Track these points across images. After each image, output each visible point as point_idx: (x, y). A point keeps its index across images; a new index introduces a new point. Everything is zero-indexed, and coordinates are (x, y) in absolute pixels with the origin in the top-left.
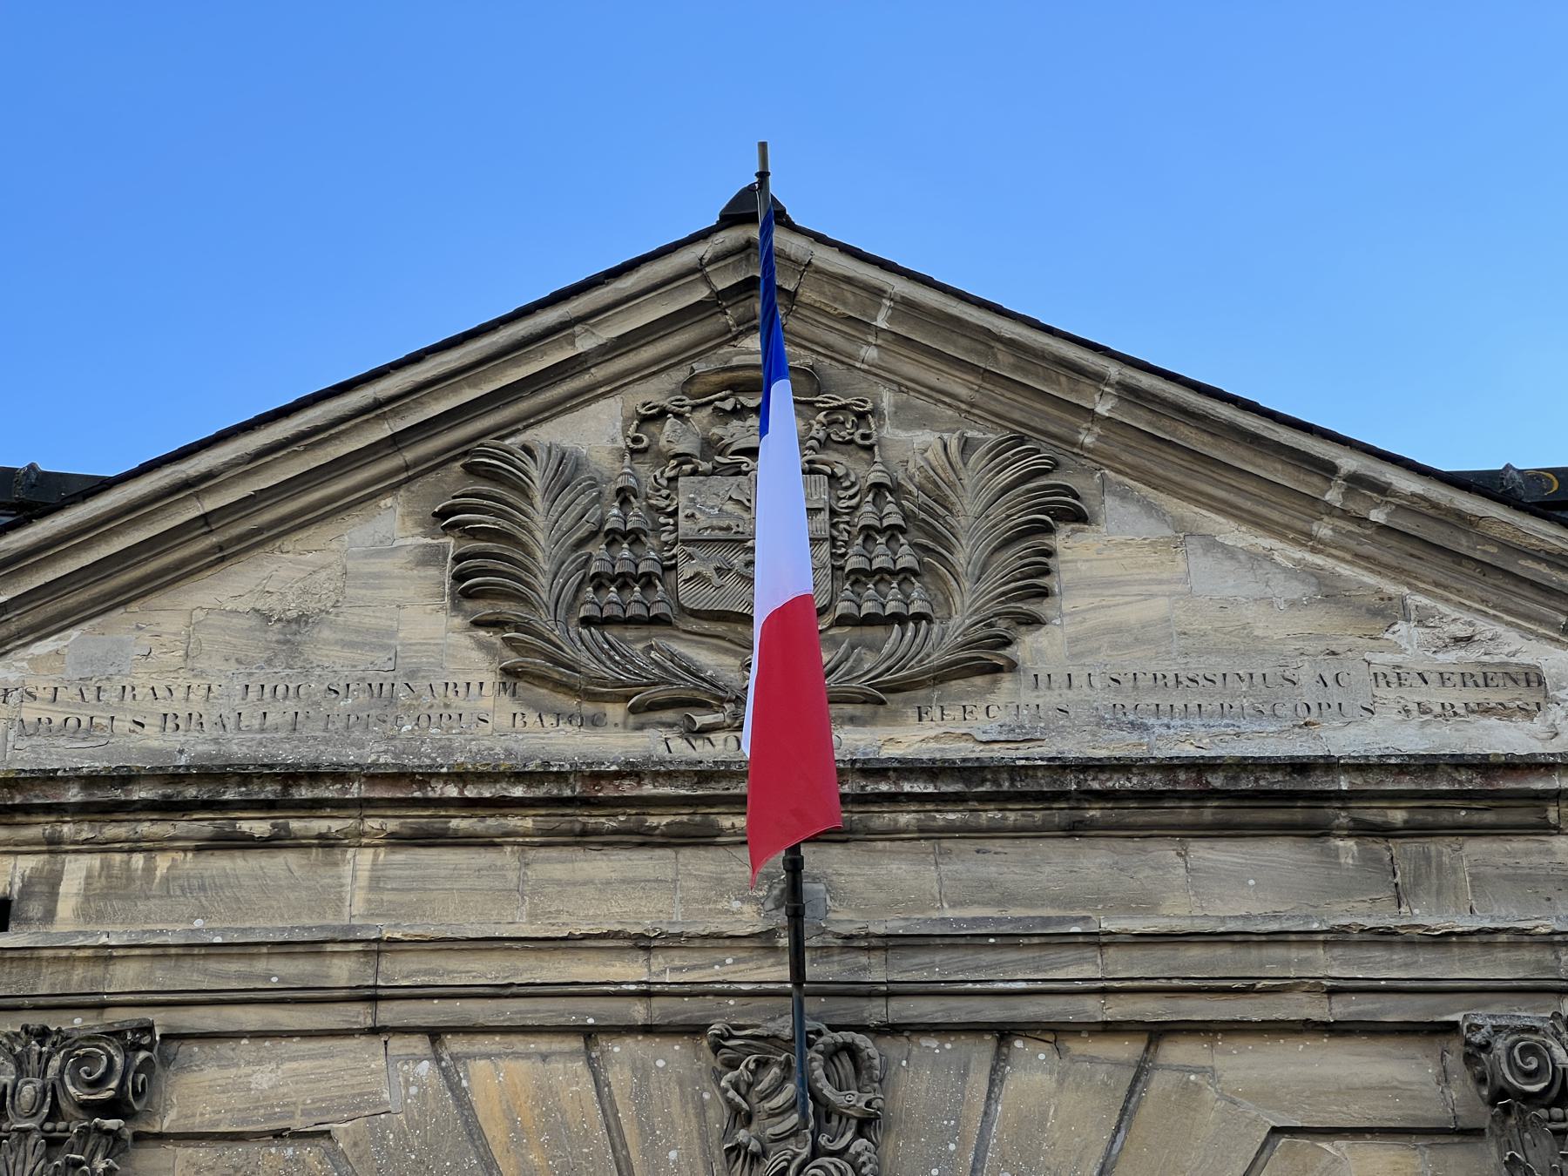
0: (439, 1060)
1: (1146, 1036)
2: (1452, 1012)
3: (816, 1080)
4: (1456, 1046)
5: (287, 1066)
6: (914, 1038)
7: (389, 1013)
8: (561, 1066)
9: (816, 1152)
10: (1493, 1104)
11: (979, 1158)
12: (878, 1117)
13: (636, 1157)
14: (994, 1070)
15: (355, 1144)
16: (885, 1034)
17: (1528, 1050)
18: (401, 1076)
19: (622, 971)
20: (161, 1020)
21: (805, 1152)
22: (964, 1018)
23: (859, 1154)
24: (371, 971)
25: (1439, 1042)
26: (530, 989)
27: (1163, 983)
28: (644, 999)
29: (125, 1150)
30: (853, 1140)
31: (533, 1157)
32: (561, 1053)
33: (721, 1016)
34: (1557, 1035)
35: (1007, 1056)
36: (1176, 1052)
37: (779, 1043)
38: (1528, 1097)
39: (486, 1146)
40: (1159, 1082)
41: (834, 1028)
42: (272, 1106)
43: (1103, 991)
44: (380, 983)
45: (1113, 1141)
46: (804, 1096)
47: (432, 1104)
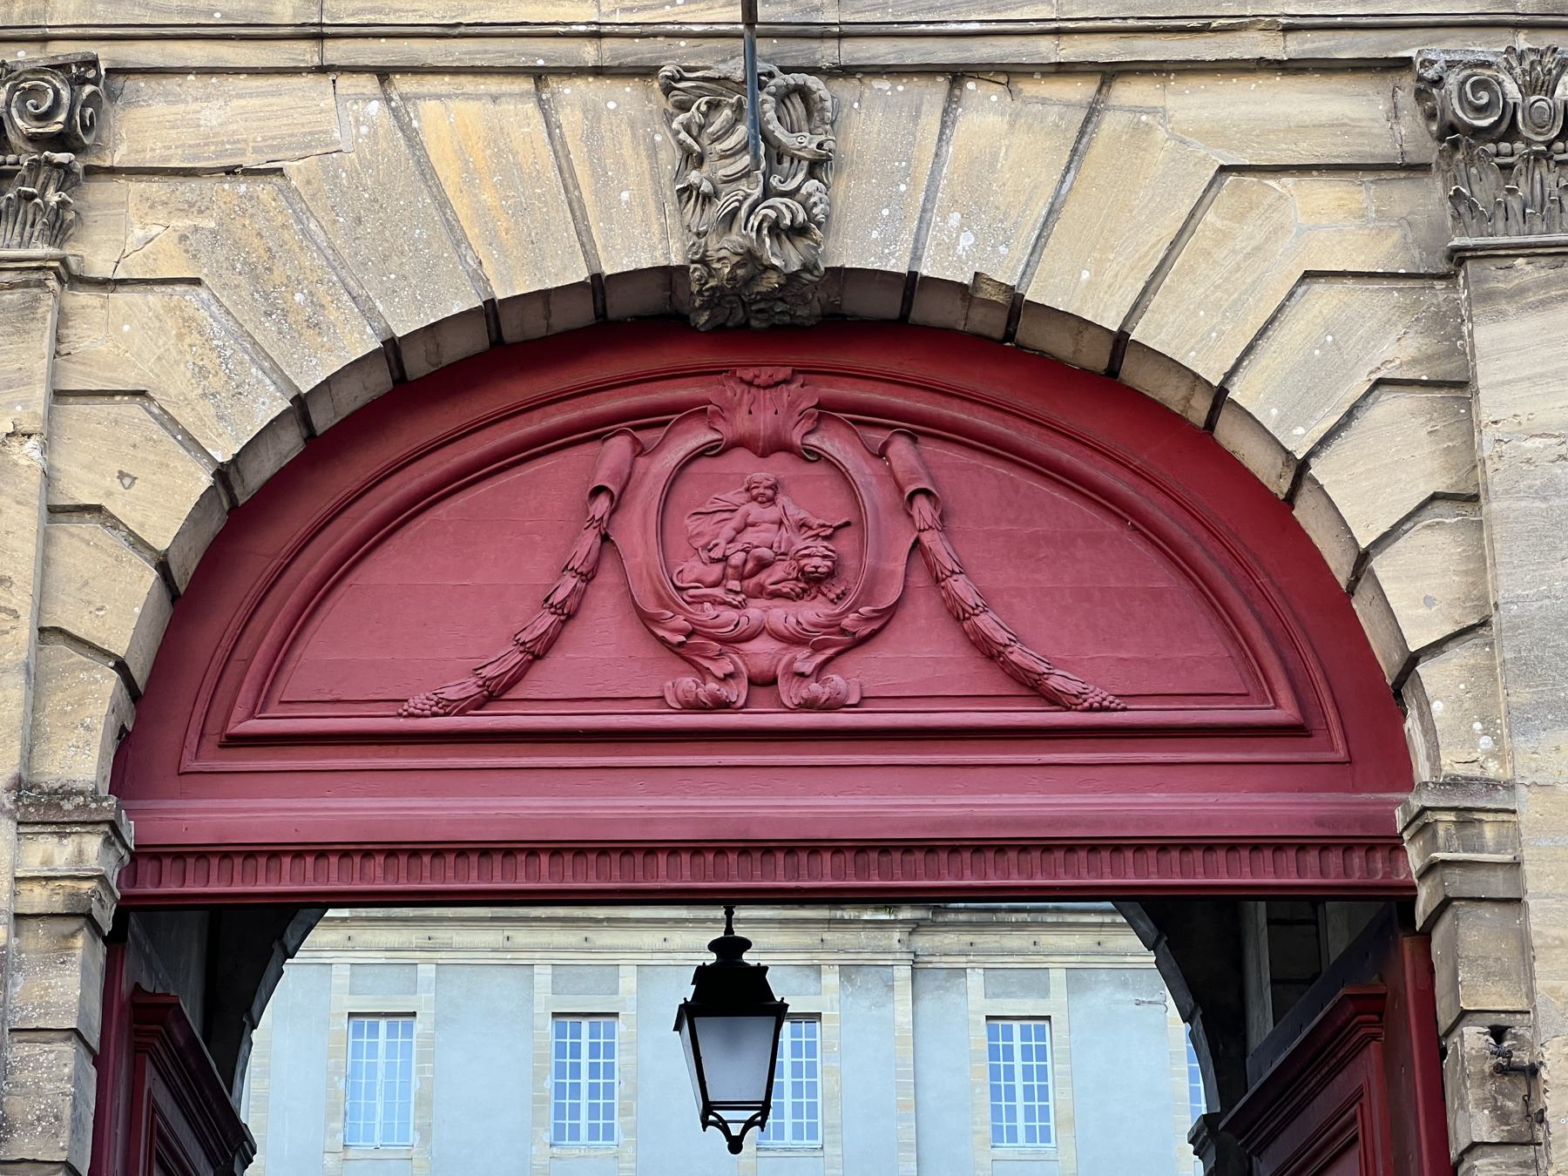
0: (388, 100)
1: (1098, 78)
2: (1405, 48)
3: (768, 122)
4: (1408, 81)
5: (235, 103)
6: (866, 80)
7: (336, 52)
8: (512, 107)
9: (767, 192)
10: (1441, 139)
11: (929, 198)
12: (830, 159)
13: (588, 198)
14: (946, 112)
15: (308, 182)
16: (837, 76)
17: (1481, 85)
18: (349, 115)
19: (571, 11)
20: (107, 54)
21: (757, 192)
22: (917, 60)
23: (810, 195)
24: (315, 9)
25: (1391, 79)
26: (479, 30)
27: (1118, 23)
28: (595, 41)
29: (77, 184)
30: (804, 181)
31: (487, 197)
32: (511, 95)
33: (673, 57)
34: (1510, 69)
35: (959, 98)
36: (1128, 92)
37: (730, 85)
38: (1477, 132)
39: (439, 186)
40: (1110, 123)
41: (786, 70)
42: (223, 143)
43: (1058, 32)
44: (325, 21)
45: (1062, 182)
46: (756, 138)
47: (383, 145)
